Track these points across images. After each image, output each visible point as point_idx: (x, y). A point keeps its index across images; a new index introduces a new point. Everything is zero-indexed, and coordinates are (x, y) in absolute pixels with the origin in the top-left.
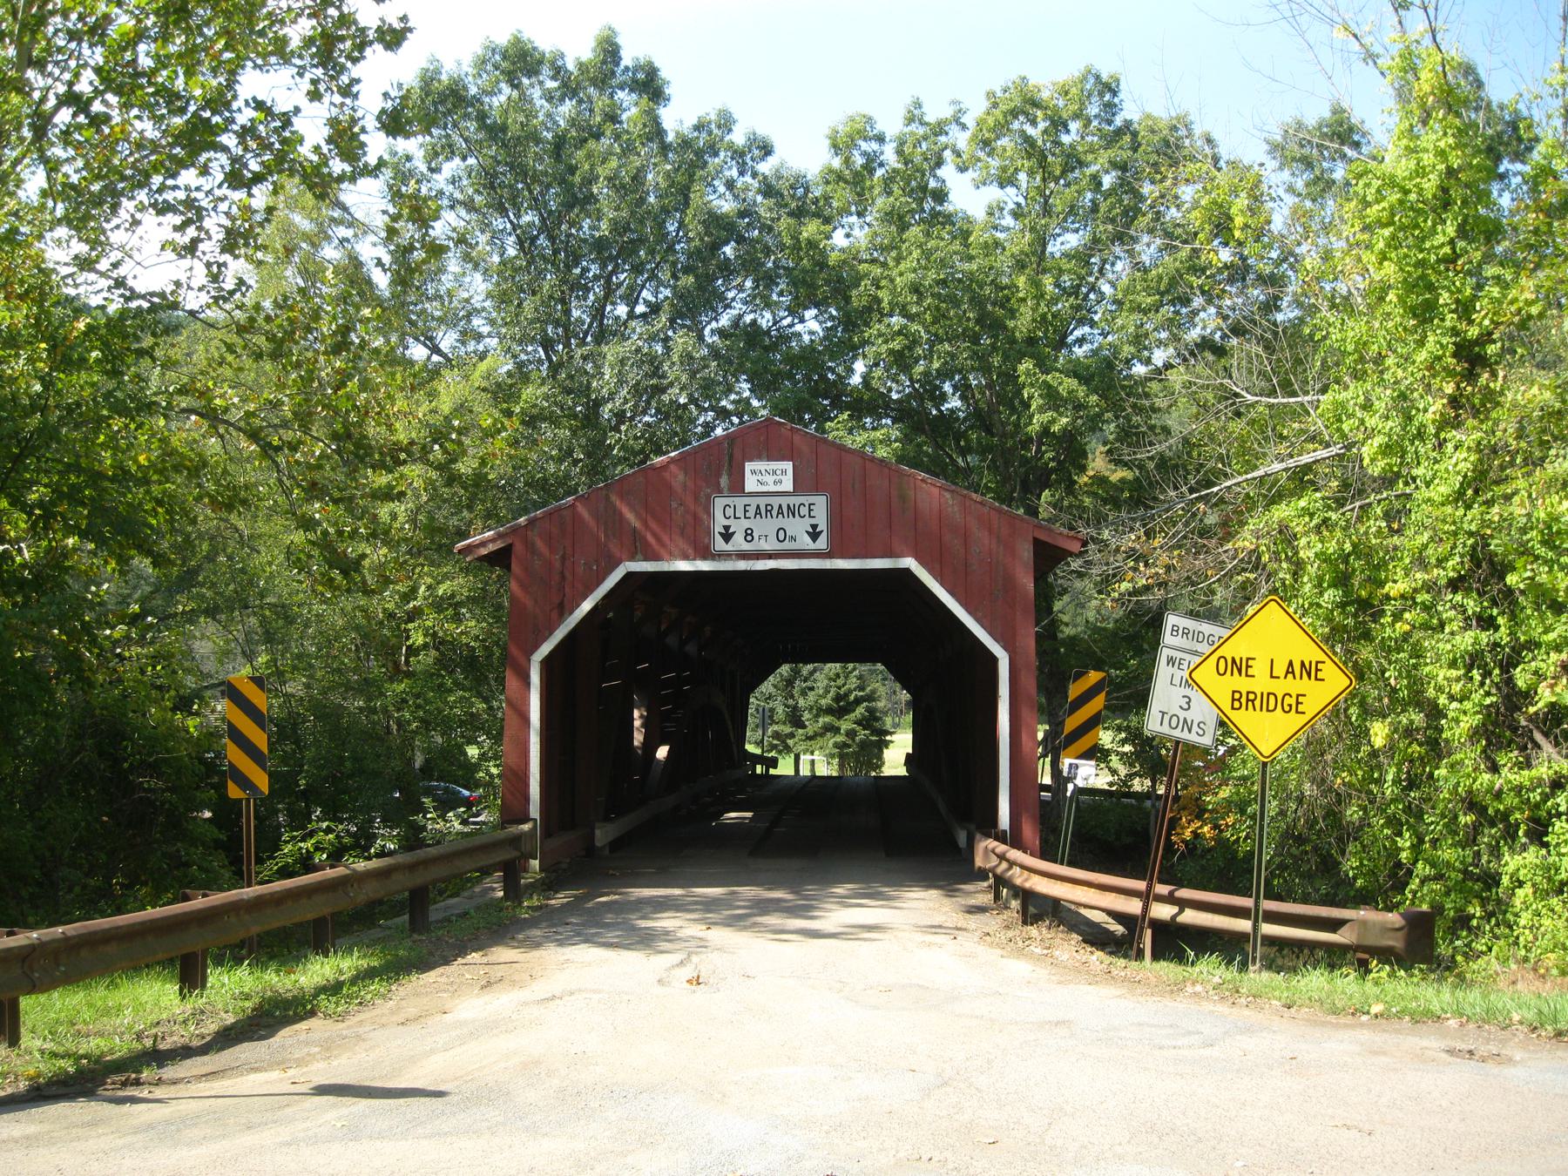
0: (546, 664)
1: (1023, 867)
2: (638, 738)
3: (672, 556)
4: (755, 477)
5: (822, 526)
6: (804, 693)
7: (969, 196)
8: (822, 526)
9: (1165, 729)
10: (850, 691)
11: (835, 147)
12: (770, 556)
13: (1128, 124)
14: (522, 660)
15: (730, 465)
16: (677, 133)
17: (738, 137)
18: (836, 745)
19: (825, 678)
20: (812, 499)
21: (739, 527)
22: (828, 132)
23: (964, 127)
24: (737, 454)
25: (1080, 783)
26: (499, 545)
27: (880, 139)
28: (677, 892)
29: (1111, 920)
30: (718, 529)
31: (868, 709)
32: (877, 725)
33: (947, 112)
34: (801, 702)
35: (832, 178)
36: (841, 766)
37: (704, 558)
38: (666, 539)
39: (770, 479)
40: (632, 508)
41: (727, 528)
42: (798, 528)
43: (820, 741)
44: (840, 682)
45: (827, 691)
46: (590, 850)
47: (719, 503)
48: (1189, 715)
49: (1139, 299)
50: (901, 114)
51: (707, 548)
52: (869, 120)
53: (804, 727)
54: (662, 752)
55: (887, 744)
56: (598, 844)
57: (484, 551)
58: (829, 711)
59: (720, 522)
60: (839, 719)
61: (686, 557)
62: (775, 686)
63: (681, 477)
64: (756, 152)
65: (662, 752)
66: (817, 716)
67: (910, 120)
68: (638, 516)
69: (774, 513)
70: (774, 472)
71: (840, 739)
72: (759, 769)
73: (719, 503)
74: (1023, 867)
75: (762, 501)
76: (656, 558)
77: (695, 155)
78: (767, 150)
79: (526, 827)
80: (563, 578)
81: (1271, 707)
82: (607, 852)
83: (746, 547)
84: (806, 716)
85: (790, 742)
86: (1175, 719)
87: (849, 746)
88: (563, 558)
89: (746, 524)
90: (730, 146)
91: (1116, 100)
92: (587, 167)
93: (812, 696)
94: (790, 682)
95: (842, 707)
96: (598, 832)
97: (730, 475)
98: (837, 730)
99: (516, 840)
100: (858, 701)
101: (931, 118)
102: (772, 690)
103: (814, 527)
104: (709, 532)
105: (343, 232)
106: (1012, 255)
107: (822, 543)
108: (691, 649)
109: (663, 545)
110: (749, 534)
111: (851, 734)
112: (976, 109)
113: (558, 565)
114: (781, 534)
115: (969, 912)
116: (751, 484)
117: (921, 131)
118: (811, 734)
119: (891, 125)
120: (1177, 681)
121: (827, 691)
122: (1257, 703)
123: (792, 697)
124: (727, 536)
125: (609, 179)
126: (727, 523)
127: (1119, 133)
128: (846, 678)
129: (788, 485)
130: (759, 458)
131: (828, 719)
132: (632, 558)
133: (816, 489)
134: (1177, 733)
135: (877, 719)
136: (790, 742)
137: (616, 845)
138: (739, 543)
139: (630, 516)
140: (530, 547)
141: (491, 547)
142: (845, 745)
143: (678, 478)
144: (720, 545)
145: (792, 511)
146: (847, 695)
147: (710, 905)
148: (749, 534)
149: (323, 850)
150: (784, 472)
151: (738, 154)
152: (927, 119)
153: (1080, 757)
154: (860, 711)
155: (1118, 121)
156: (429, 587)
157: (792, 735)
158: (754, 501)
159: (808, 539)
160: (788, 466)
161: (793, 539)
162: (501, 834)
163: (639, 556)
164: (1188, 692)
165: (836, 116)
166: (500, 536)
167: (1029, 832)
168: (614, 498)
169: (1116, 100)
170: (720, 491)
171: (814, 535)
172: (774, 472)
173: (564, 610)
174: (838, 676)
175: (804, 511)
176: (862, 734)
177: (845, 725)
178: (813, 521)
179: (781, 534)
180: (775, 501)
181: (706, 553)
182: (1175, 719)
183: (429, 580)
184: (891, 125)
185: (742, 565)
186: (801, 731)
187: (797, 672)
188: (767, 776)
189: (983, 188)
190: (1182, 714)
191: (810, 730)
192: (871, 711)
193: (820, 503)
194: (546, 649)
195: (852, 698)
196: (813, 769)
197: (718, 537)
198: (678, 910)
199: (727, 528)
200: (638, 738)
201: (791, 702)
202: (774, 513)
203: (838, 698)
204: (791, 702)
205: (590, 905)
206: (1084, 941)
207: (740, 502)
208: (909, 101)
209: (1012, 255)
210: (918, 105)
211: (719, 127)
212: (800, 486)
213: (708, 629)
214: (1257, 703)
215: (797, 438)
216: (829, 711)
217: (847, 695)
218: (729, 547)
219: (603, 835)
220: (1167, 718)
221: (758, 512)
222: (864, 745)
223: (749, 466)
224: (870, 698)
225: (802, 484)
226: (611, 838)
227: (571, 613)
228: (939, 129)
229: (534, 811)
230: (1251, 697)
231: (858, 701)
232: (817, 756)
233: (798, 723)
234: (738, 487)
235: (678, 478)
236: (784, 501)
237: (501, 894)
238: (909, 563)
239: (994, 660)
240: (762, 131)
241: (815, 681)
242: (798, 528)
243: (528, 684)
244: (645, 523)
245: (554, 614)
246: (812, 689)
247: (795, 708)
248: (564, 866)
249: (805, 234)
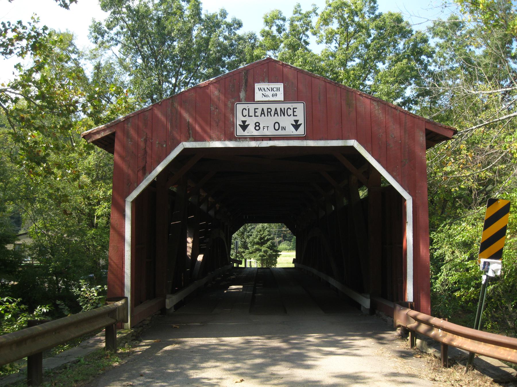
0: (136, 203)
1: (444, 329)
2: (189, 252)
3: (212, 139)
5: (301, 121)
6: (248, 237)
7: (317, 47)
8: (301, 121)
10: (265, 236)
11: (267, 22)
12: (270, 138)
13: (380, 15)
14: (120, 201)
15: (246, 85)
16: (206, 15)
17: (229, 20)
18: (260, 256)
19: (257, 230)
20: (295, 105)
21: (251, 122)
22: (263, 16)
23: (317, 14)
24: (250, 80)
25: (491, 274)
26: (108, 133)
27: (284, 20)
28: (213, 341)
29: (504, 365)
30: (239, 122)
31: (272, 243)
32: (275, 248)
33: (310, 9)
34: (247, 240)
35: (265, 34)
36: (262, 264)
37: (230, 139)
38: (208, 129)
39: (270, 93)
40: (188, 111)
41: (244, 122)
42: (287, 122)
43: (254, 254)
44: (261, 233)
45: (257, 236)
46: (163, 310)
47: (240, 107)
49: (387, 79)
50: (292, 9)
51: (233, 133)
52: (280, 12)
53: (248, 249)
54: (200, 258)
55: (279, 255)
56: (168, 307)
57: (98, 137)
58: (258, 243)
60: (261, 246)
61: (219, 139)
62: (237, 234)
63: (216, 93)
64: (236, 26)
65: (200, 258)
66: (253, 245)
67: (296, 12)
68: (191, 115)
69: (273, 113)
70: (272, 89)
71: (262, 253)
72: (235, 265)
73: (240, 107)
74: (444, 329)
75: (265, 107)
76: (202, 140)
77: (212, 24)
78: (240, 25)
79: (120, 303)
80: (146, 152)
82: (173, 310)
83: (256, 133)
84: (249, 245)
85: (243, 254)
87: (265, 256)
88: (146, 141)
89: (255, 120)
90: (226, 23)
91: (376, 5)
92: (170, 27)
93: (251, 238)
94: (243, 233)
95: (262, 242)
96: (167, 301)
97: (246, 91)
98: (260, 250)
99: (112, 312)
100: (268, 240)
101: (304, 12)
102: (237, 236)
103: (296, 121)
104: (233, 125)
105: (73, 56)
106: (340, 60)
107: (301, 131)
108: (211, 213)
109: (205, 131)
110: (257, 126)
111: (265, 252)
112: (322, 7)
113: (142, 144)
114: (277, 125)
115: (402, 357)
116: (258, 96)
117: (300, 16)
118: (251, 251)
119: (288, 14)
121: (257, 236)
123: (244, 238)
124: (244, 127)
125: (179, 30)
126: (244, 119)
127: (376, 17)
128: (264, 231)
129: (280, 96)
130: (263, 81)
131: (257, 246)
132: (187, 140)
133: (297, 99)
135: (275, 246)
136: (243, 254)
137: (177, 307)
138: (251, 131)
139: (186, 116)
140: (126, 133)
141: (103, 134)
142: (263, 256)
143: (215, 93)
144: (240, 132)
145: (283, 112)
146: (264, 238)
147: (238, 354)
148: (257, 126)
149: (9, 312)
150: (278, 89)
151: (229, 26)
152: (301, 12)
153: (491, 257)
154: (269, 243)
155: (377, 13)
156: (104, 192)
157: (244, 252)
158: (260, 106)
159: (293, 129)
160: (281, 86)
161: (284, 128)
162: (102, 308)
163: (191, 139)
165: (268, 10)
166: (108, 127)
167: (424, 303)
168: (176, 105)
169: (376, 5)
170: (239, 100)
171: (296, 126)
172: (272, 89)
173: (145, 171)
174: (261, 231)
175: (290, 112)
176: (270, 252)
177: (263, 248)
178: (296, 118)
179: (277, 125)
180: (273, 106)
181: (231, 137)
183: (104, 189)
184: (288, 14)
185: (253, 144)
186: (247, 251)
187: (245, 229)
188: (238, 267)
189: (320, 44)
191: (251, 250)
192: (273, 243)
193: (300, 108)
194: (135, 194)
195: (266, 239)
196: (250, 265)
197: (238, 127)
198: (218, 360)
199: (244, 122)
200: (189, 252)
201: (243, 240)
202: (273, 113)
203: (261, 239)
204: (243, 240)
205: (159, 354)
206: (495, 381)
207: (252, 107)
208: (296, 4)
209: (340, 60)
210: (299, 6)
211: (221, 16)
212: (287, 98)
215: (286, 70)
216: (258, 243)
217: (264, 238)
218: (246, 133)
219: (170, 302)
222: (270, 256)
223: (257, 86)
224: (273, 239)
226: (174, 304)
227: (150, 172)
228: (307, 15)
229: (128, 293)
231: (268, 240)
232: (252, 260)
233: (246, 248)
234: (251, 98)
235: (215, 93)
236: (279, 106)
237: (104, 345)
238: (353, 143)
239: (401, 200)
240: (238, 18)
241: (252, 232)
242: (287, 122)
243: (124, 216)
244: (195, 120)
245: (140, 174)
246: (251, 235)
247: (245, 242)
248: (147, 322)
249: (255, 53)
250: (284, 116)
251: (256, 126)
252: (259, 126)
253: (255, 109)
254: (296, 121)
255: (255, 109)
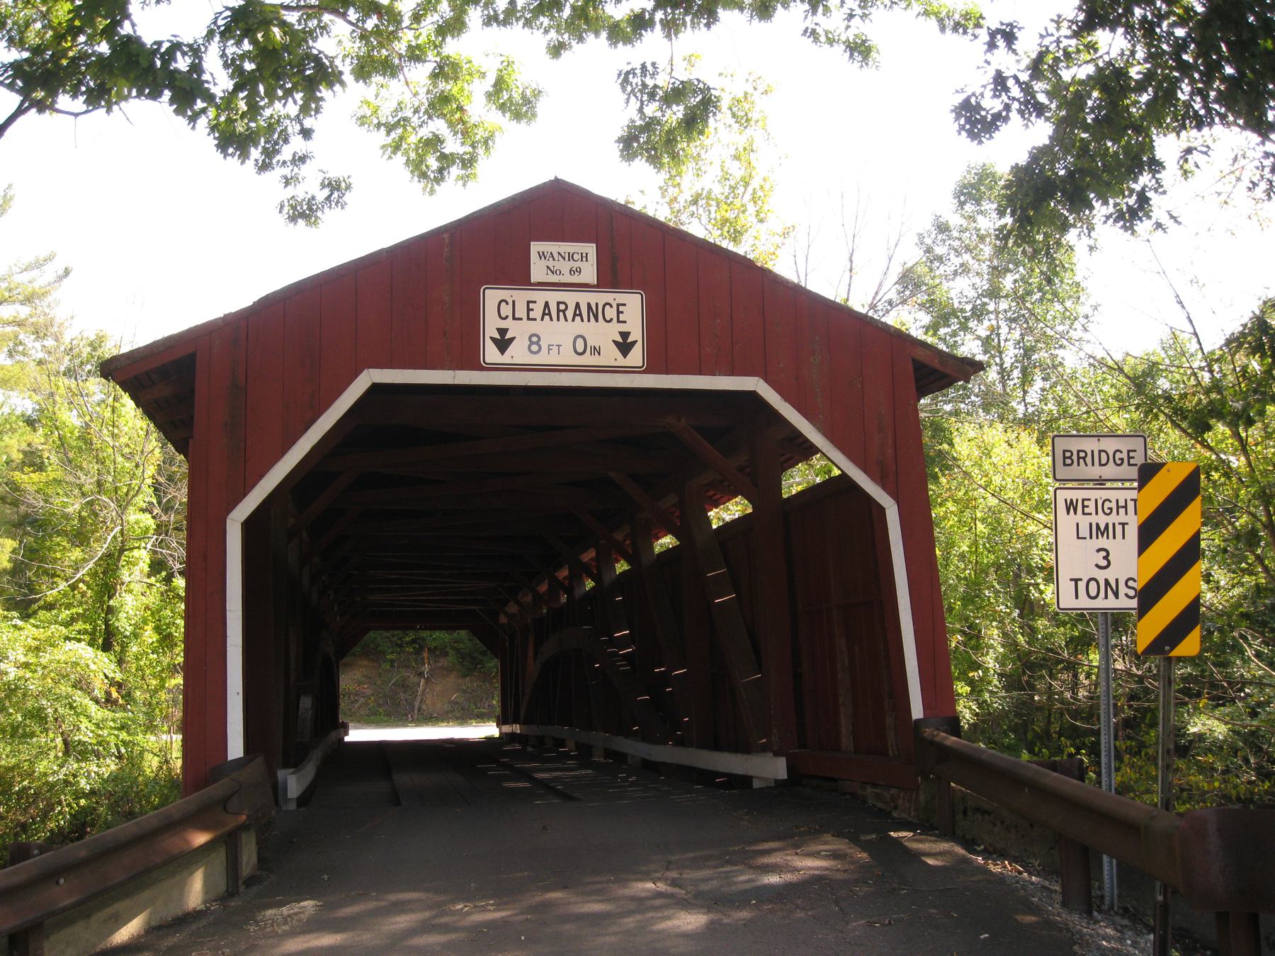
4: (544, 263)
8: (636, 334)
9: (1084, 602)
39: (565, 266)
41: (503, 332)
42: (603, 335)
48: (1110, 574)
59: (491, 325)
69: (570, 313)
70: (571, 257)
75: (553, 297)
81: (1104, 461)
86: (1093, 585)
103: (625, 335)
107: (636, 357)
110: (534, 340)
116: (538, 272)
120: (1084, 532)
122: (1089, 459)
124: (503, 343)
126: (503, 324)
129: (589, 274)
134: (1100, 603)
138: (518, 353)
148: (534, 340)
150: (585, 257)
158: (541, 297)
160: (591, 249)
164: (1103, 542)
171: (624, 346)
172: (571, 257)
175: (611, 313)
178: (624, 328)
179: (580, 343)
180: (571, 298)
182: (1093, 585)
190: (1101, 576)
193: (633, 304)
199: (503, 332)
202: (570, 313)
207: (521, 296)
213: (158, 63)
214: (1089, 459)
218: (506, 359)
220: (1082, 585)
221: (546, 311)
223: (535, 247)
225: (610, 278)
230: (1082, 454)
236: (584, 298)
250: (597, 320)
251: (532, 343)
252: (538, 343)
253: (528, 302)
254: (625, 335)
255: (528, 302)
